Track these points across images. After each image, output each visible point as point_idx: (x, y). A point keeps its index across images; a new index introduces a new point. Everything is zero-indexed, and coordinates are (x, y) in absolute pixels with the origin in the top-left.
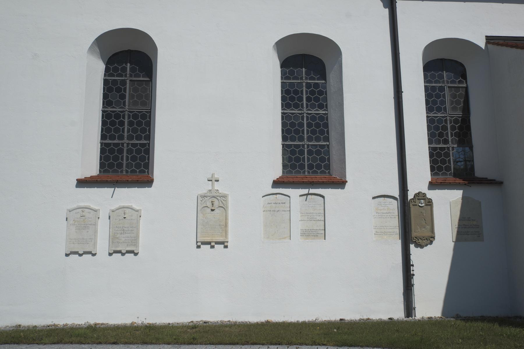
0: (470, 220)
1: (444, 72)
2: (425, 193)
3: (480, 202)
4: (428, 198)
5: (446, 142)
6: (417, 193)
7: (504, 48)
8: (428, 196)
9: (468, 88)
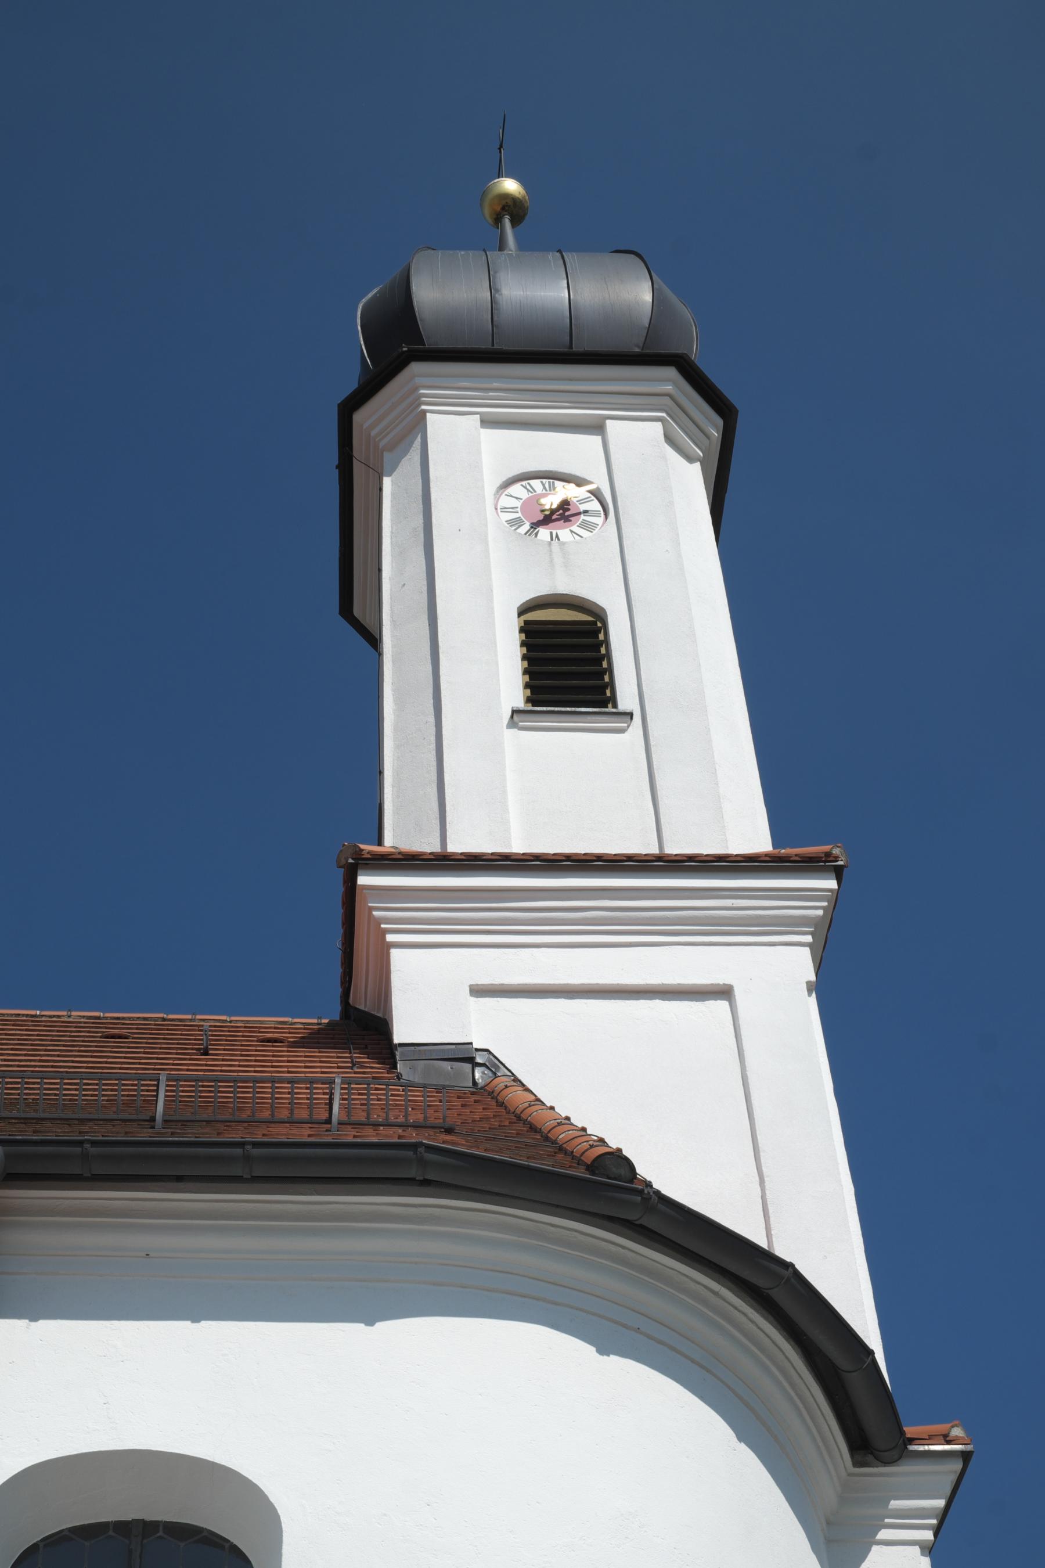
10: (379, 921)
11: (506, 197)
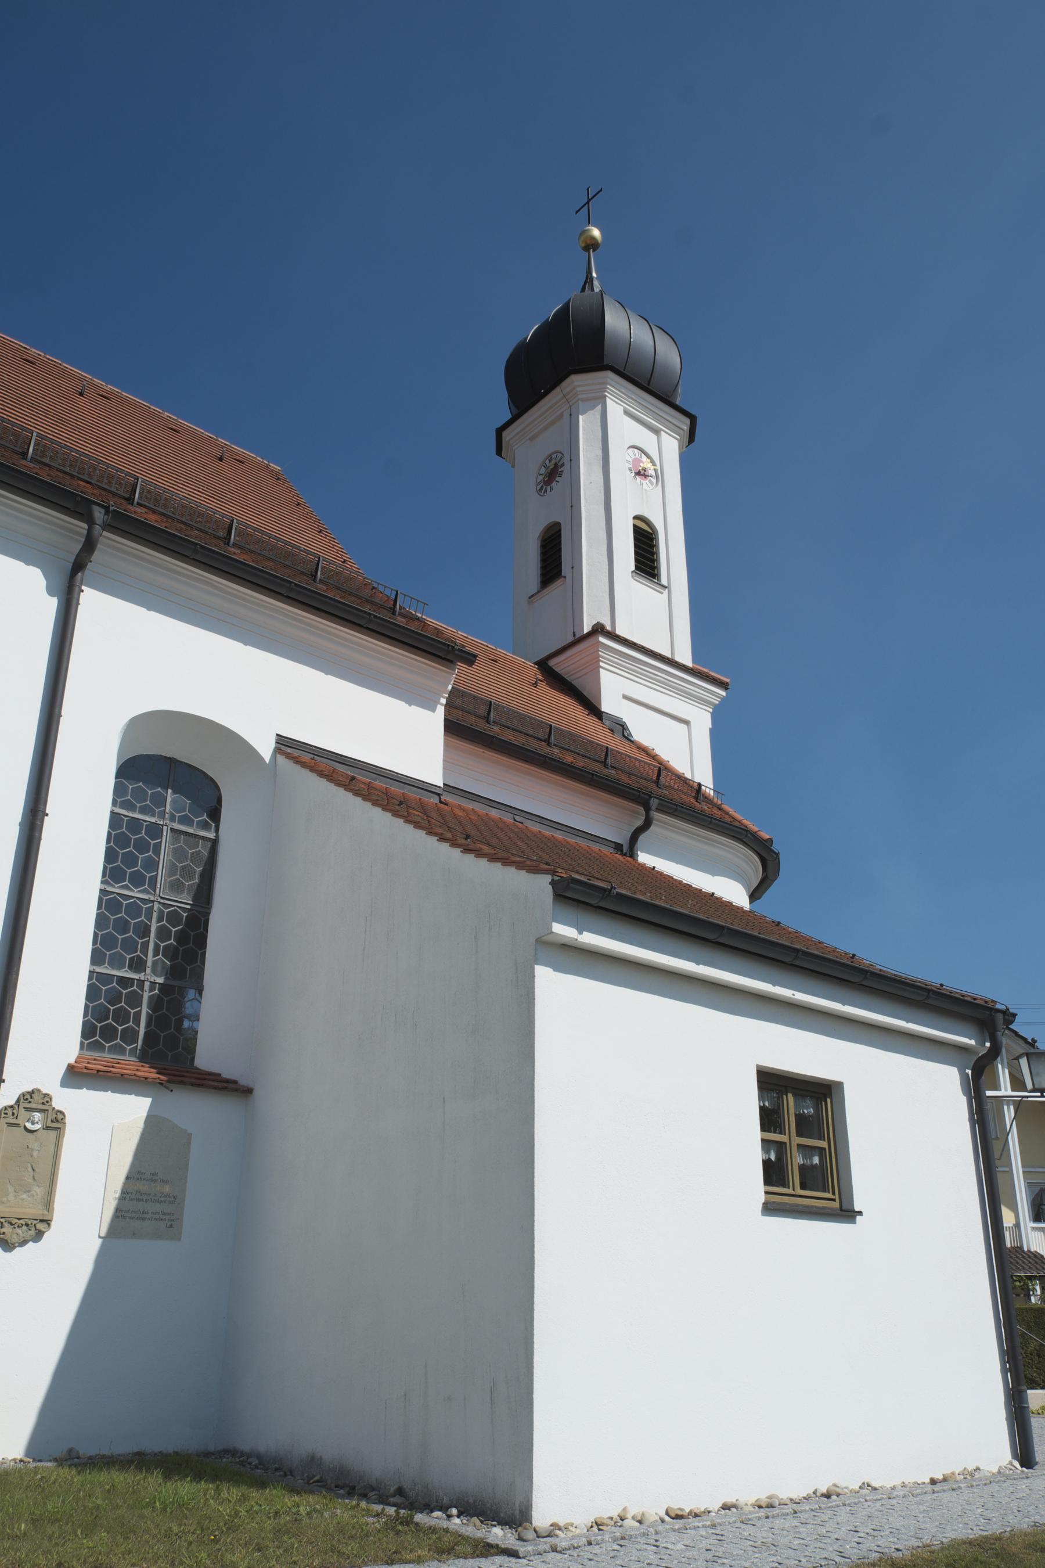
0: (156, 1181)
1: (170, 791)
2: (50, 1093)
3: (190, 1135)
4: (54, 1108)
5: (138, 965)
6: (28, 1093)
7: (306, 773)
8: (57, 1104)
9: (218, 842)
10: (599, 656)
11: (593, 238)
